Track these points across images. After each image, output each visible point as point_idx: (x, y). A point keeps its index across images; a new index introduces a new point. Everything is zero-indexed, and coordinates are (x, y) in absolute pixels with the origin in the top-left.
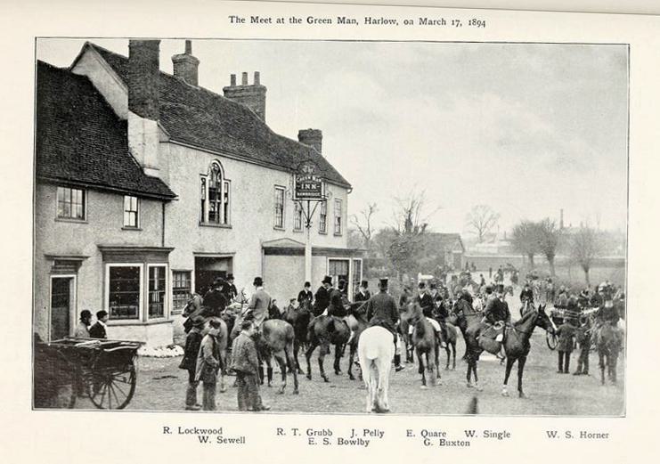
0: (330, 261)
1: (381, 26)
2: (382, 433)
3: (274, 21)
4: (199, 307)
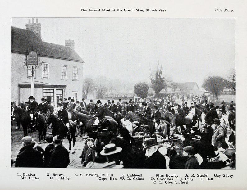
0: (56, 90)
2: (232, 176)
3: (111, 10)
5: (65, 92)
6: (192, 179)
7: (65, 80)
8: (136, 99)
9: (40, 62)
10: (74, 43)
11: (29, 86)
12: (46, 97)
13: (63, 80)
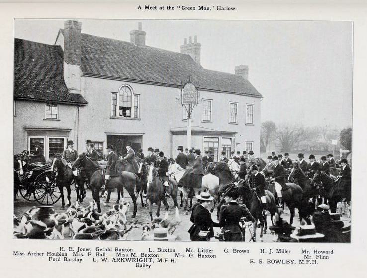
1: (226, 12)
3: (158, 8)
4: (67, 164)
5: (234, 141)
6: (150, 266)
7: (235, 124)
8: (343, 154)
9: (199, 99)
10: (248, 70)
11: (184, 133)
12: (208, 149)
13: (231, 123)
